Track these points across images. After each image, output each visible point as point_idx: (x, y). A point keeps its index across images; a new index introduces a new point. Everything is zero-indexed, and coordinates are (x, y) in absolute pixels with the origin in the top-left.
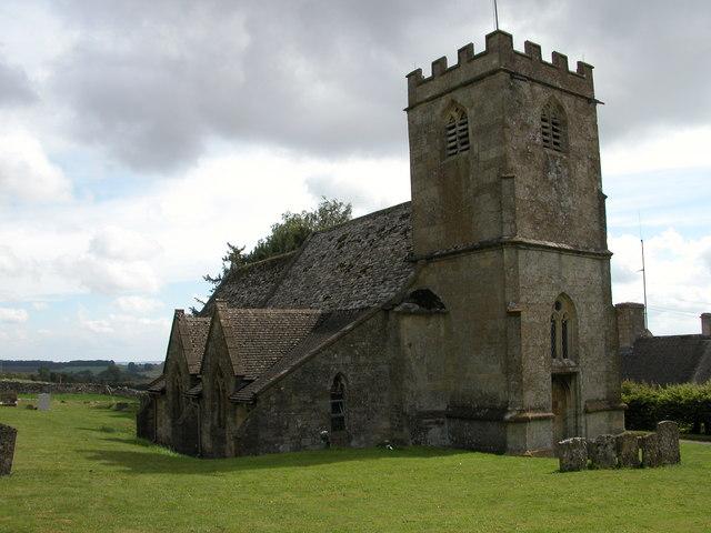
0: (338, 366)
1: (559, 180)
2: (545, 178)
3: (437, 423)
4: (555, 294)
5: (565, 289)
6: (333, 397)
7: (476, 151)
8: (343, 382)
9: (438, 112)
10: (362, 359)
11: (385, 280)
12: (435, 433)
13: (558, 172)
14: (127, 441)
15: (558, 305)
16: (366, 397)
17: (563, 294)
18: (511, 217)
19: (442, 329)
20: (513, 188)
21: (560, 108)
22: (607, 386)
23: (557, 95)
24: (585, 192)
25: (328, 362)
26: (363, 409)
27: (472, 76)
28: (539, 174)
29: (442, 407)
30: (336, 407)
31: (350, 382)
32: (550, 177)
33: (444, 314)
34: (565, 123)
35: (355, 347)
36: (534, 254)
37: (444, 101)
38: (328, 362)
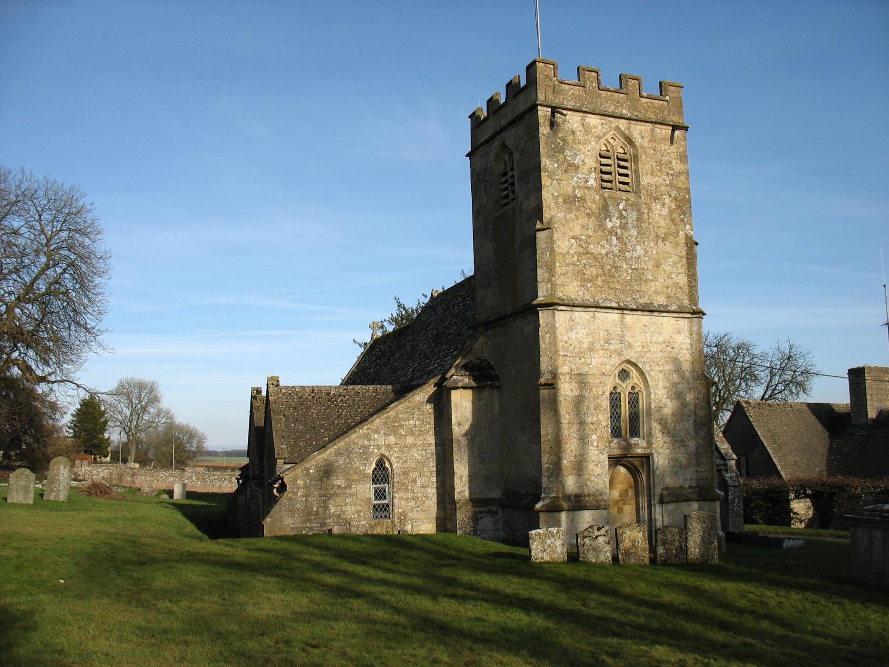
0: (379, 447)
1: (624, 227)
2: (602, 227)
3: (490, 512)
4: (615, 361)
5: (632, 355)
6: (375, 481)
7: (520, 200)
8: (387, 465)
9: (492, 156)
10: (410, 440)
11: (439, 352)
12: (652, 555)
13: (621, 217)
14: (407, 588)
15: (624, 375)
16: (415, 481)
17: (628, 362)
18: (547, 275)
19: (497, 405)
20: (551, 241)
21: (630, 141)
22: (697, 471)
23: (623, 124)
24: (663, 240)
25: (366, 443)
26: (410, 495)
27: (517, 114)
28: (592, 223)
29: (496, 494)
30: (380, 494)
31: (396, 465)
32: (609, 225)
33: (499, 387)
34: (636, 159)
35: (402, 426)
36: (581, 315)
37: (496, 143)
38: (366, 443)
